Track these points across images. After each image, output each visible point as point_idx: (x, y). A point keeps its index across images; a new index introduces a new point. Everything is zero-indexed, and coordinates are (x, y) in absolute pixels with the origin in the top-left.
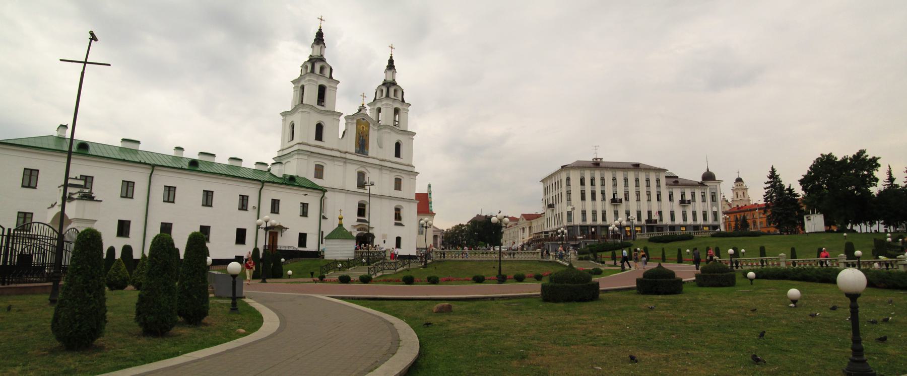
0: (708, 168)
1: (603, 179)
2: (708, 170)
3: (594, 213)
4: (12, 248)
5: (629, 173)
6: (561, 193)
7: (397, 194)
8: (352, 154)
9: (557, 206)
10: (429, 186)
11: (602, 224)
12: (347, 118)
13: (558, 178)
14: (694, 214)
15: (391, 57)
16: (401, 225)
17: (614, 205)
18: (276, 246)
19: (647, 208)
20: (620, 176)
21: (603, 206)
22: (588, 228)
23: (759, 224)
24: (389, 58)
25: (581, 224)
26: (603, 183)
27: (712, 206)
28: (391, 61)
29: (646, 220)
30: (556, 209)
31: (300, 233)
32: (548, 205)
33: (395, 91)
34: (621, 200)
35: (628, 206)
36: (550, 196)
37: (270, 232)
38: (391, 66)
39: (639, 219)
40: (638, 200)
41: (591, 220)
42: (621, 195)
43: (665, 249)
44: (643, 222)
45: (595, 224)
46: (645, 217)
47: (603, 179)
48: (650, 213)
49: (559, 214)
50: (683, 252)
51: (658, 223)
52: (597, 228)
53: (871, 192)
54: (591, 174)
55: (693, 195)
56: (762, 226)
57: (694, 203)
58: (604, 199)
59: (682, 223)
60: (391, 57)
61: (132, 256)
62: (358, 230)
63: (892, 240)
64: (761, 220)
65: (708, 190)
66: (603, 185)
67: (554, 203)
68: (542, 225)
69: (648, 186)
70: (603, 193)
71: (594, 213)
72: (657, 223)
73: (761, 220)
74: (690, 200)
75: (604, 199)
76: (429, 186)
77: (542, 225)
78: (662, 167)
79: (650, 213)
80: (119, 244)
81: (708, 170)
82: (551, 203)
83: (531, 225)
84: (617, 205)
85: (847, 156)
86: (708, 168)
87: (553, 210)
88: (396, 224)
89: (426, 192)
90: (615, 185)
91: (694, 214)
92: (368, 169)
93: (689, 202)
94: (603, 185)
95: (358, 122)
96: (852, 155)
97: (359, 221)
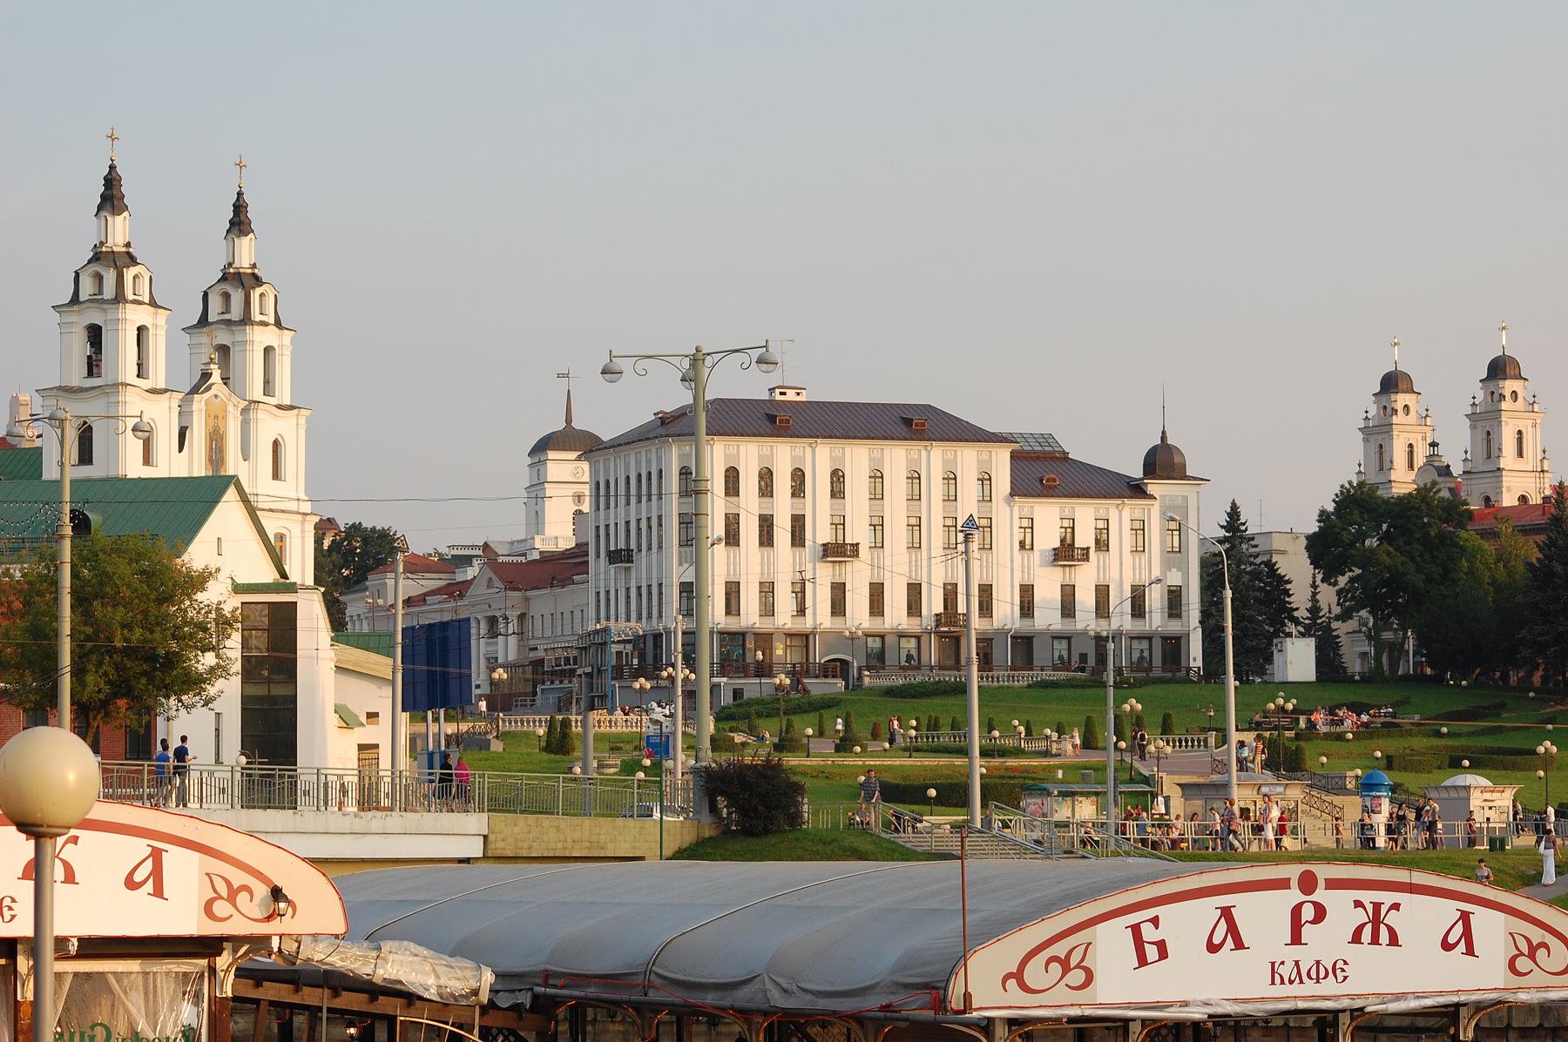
0: (1164, 432)
2: (1164, 437)
3: (767, 589)
6: (660, 517)
9: (642, 559)
13: (627, 466)
26: (879, 491)
30: (639, 570)
32: (609, 553)
34: (855, 550)
36: (618, 515)
42: (859, 532)
43: (412, 706)
46: (933, 603)
49: (649, 586)
50: (833, 711)
52: (747, 636)
53: (1282, 574)
54: (871, 459)
61: (1318, 648)
67: (633, 546)
68: (577, 615)
71: (767, 589)
77: (577, 615)
80: (1399, 406)
81: (1164, 437)
82: (622, 545)
83: (527, 607)
85: (1342, 486)
86: (1164, 432)
87: (627, 569)
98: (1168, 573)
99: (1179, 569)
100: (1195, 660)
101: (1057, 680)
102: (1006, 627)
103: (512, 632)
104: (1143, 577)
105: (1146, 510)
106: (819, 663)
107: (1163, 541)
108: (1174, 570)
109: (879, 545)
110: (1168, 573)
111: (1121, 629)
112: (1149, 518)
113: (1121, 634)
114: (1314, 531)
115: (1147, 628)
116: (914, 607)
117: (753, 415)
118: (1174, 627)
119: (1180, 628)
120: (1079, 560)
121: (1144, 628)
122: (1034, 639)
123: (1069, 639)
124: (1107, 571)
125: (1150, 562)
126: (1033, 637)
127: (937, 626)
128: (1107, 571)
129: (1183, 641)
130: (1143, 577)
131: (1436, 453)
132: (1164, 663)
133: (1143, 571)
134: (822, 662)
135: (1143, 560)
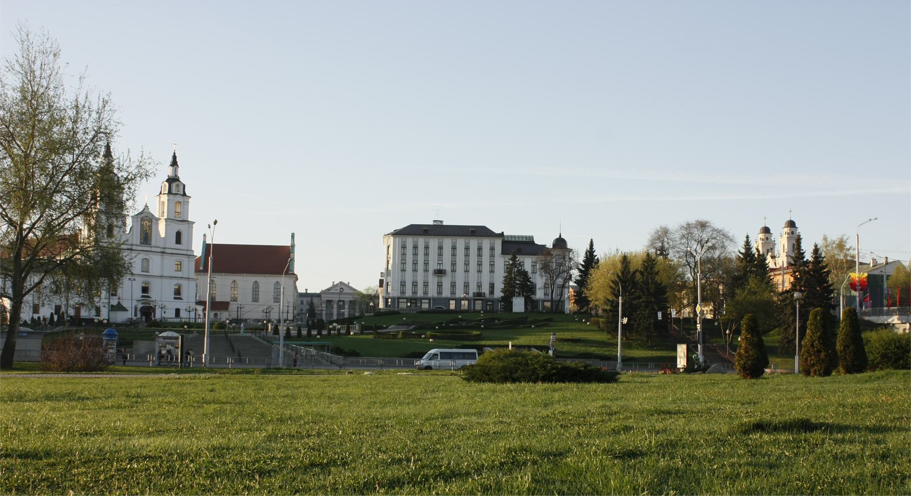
1: (427, 248)
2: (560, 236)
5: (444, 240)
7: (179, 274)
8: (137, 245)
10: (293, 236)
12: (132, 217)
14: (453, 285)
15: (174, 153)
16: (180, 299)
18: (80, 316)
19: (476, 279)
20: (461, 242)
21: (426, 277)
24: (173, 154)
25: (399, 295)
28: (174, 157)
33: (178, 185)
35: (453, 277)
37: (475, 353)
38: (174, 163)
39: (492, 292)
44: (471, 295)
47: (427, 248)
48: (479, 286)
58: (426, 270)
60: (174, 153)
62: (142, 304)
70: (426, 264)
71: (415, 284)
75: (426, 270)
76: (293, 236)
79: (479, 286)
81: (560, 236)
88: (175, 298)
89: (288, 244)
92: (151, 256)
95: (142, 220)
96: (685, 223)
97: (143, 296)
109: (453, 271)
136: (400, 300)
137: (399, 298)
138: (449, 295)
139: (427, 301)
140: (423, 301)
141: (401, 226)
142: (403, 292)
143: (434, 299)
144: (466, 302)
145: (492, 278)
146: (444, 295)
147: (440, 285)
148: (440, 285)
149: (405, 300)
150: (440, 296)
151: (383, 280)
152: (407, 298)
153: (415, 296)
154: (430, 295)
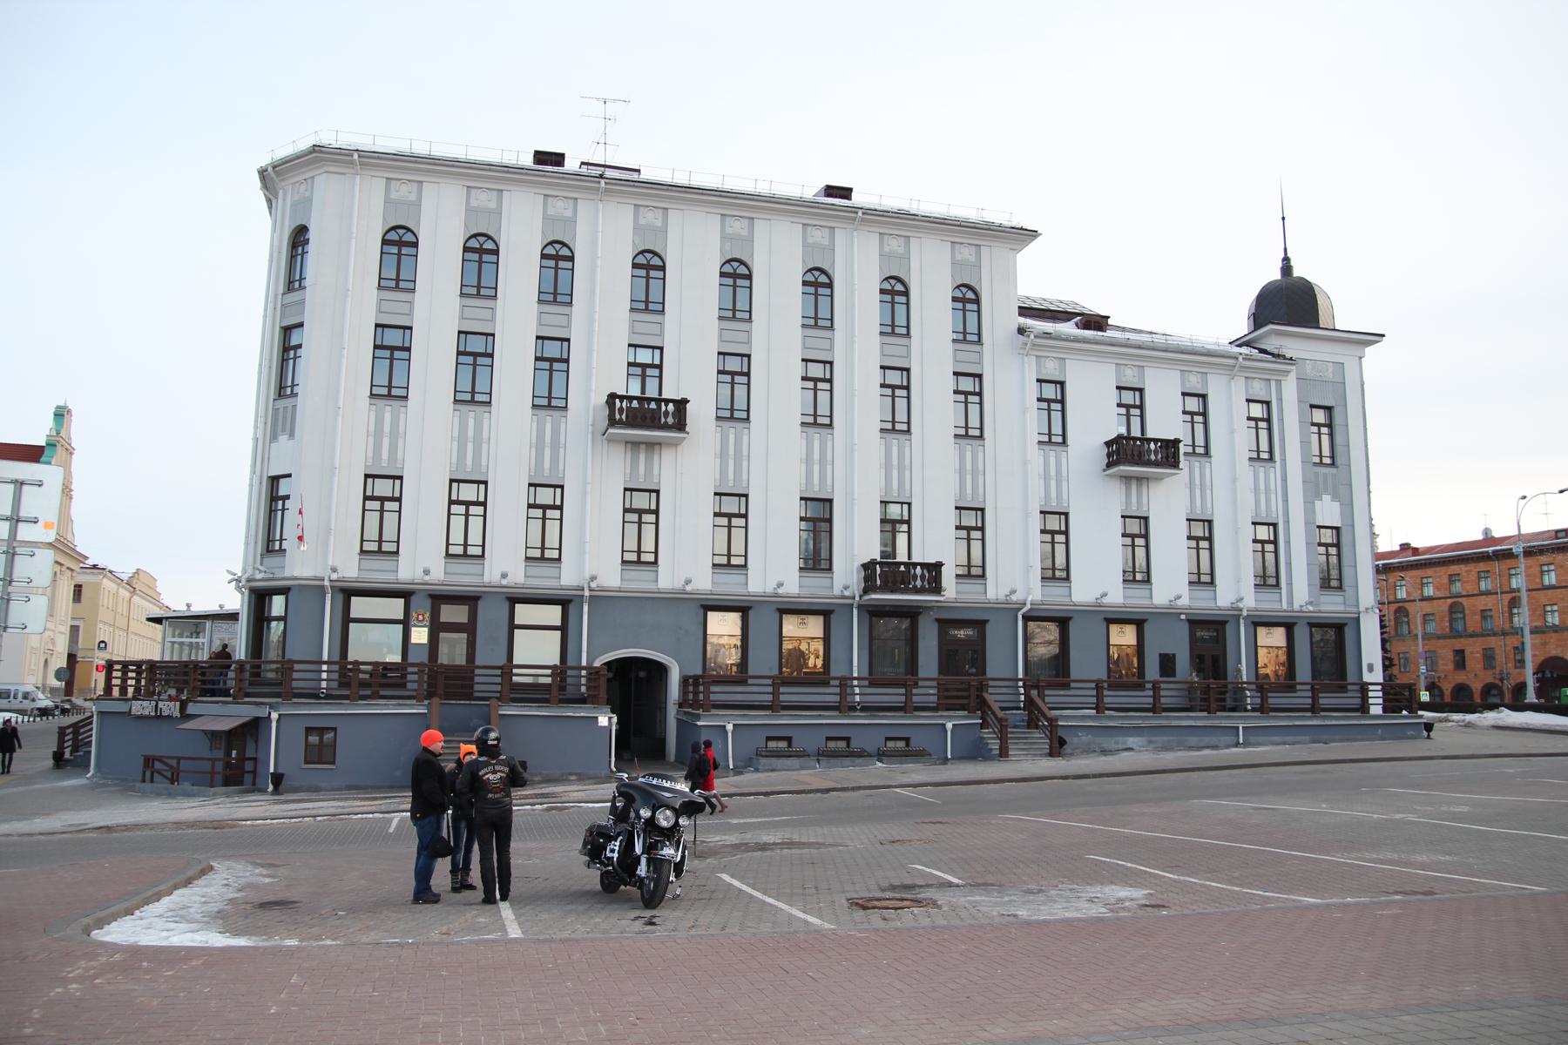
0: (1286, 259)
1: (558, 256)
2: (1287, 268)
4: (958, 690)
10: (61, 414)
11: (1184, 601)
14: (1202, 534)
17: (1127, 479)
22: (914, 629)
23: (1419, 621)
27: (1313, 492)
29: (868, 567)
31: (1161, 655)
40: (897, 428)
41: (795, 562)
44: (845, 578)
45: (1136, 600)
47: (558, 256)
51: (951, 589)
55: (1199, 410)
56: (1431, 628)
57: (1196, 463)
58: (549, 402)
59: (1117, 596)
63: (478, 774)
64: (1427, 607)
65: (1290, 387)
66: (556, 295)
69: (895, 329)
72: (937, 589)
73: (1427, 607)
74: (1176, 442)
75: (1055, 439)
76: (61, 414)
78: (1016, 222)
81: (1287, 268)
84: (652, 445)
86: (1286, 259)
90: (648, 304)
91: (1202, 534)
93: (1169, 453)
94: (556, 295)
98: (1318, 503)
99: (1335, 497)
100: (1371, 668)
101: (668, 882)
102: (1014, 598)
103: (47, 627)
104: (1274, 509)
105: (1273, 383)
106: (588, 668)
107: (1305, 443)
108: (1327, 498)
109: (734, 415)
110: (1318, 503)
111: (1241, 605)
112: (1280, 399)
113: (1238, 616)
114: (1379, 547)
115: (1285, 606)
116: (817, 560)
117: (1004, 690)
118: (1332, 606)
119: (1341, 608)
120: (1157, 464)
121: (1277, 606)
122: (1071, 623)
123: (1139, 623)
124: (1208, 492)
125: (1284, 480)
126: (1070, 618)
127: (866, 591)
128: (1208, 492)
129: (1349, 633)
130: (1274, 509)
131: (1094, 706)
132: (1315, 673)
133: (1273, 496)
134: (597, 664)
135: (1272, 475)
136: (359, 606)
137: (348, 593)
138: (704, 581)
139: (553, 614)
140: (524, 613)
141: (312, 235)
142: (381, 550)
143: (602, 600)
144: (814, 627)
145: (969, 473)
146: (668, 578)
147: (1138, 531)
148: (1138, 531)
149: (395, 607)
150: (640, 582)
151: (78, 627)
152: (404, 594)
153: (464, 578)
154: (569, 576)
